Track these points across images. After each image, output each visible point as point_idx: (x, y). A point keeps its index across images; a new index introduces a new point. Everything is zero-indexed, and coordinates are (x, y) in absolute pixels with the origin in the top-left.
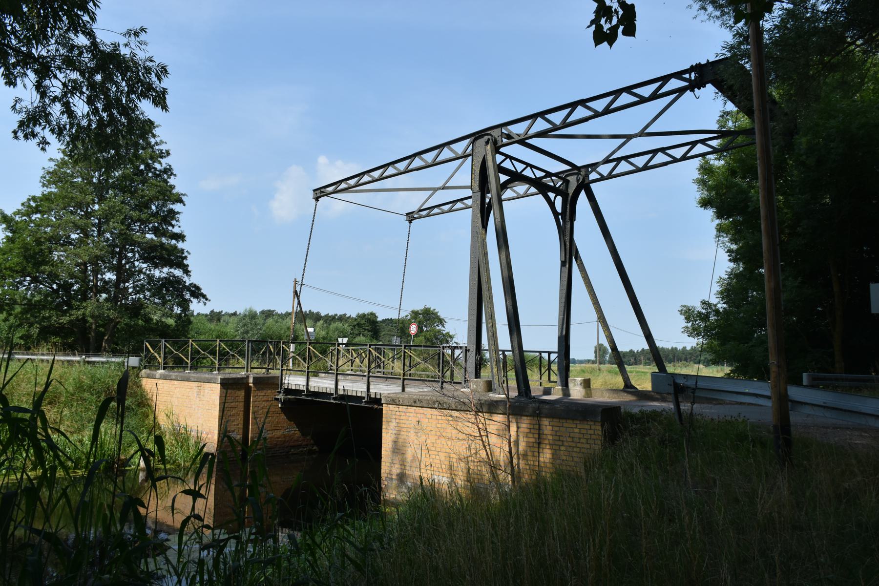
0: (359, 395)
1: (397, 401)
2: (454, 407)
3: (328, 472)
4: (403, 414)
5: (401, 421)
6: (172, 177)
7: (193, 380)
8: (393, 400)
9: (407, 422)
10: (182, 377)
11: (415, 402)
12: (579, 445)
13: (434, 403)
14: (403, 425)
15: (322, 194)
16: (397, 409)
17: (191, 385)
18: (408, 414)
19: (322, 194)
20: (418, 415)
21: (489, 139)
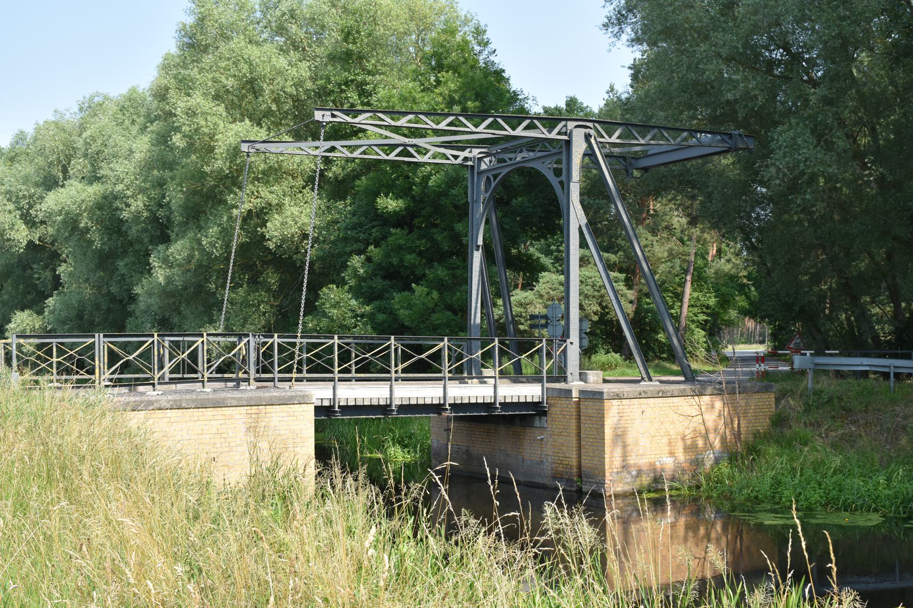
0: (382, 403)
1: (621, 395)
2: (677, 394)
3: (488, 469)
4: (627, 407)
5: (625, 414)
6: (28, 376)
7: (235, 403)
8: (617, 395)
9: (631, 414)
10: (193, 401)
11: (640, 394)
12: (763, 410)
13: (658, 392)
14: (628, 418)
15: (366, 108)
16: (620, 403)
17: (288, 410)
18: (631, 407)
19: (366, 108)
20: (642, 406)
21: (488, 178)
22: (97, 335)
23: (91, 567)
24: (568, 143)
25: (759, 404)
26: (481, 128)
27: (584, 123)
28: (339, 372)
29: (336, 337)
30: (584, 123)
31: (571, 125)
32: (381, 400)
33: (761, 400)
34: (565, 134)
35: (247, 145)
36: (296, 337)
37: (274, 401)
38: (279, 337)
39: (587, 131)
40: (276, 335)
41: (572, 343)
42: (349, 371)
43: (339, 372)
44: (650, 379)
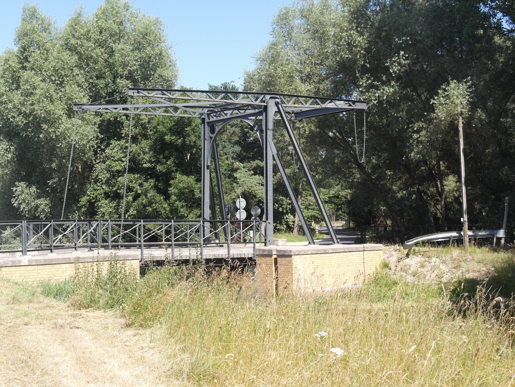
2: (355, 250)
22: (23, 221)
23: (399, 335)
24: (266, 107)
25: (374, 256)
26: (218, 100)
27: (274, 96)
28: (175, 241)
29: (173, 221)
30: (274, 96)
31: (268, 97)
32: (246, 255)
33: (375, 254)
34: (264, 102)
35: (76, 107)
36: (121, 221)
37: (327, 251)
38: (144, 221)
39: (277, 100)
40: (142, 221)
41: (269, 223)
42: (117, 242)
43: (175, 241)
44: (314, 243)
